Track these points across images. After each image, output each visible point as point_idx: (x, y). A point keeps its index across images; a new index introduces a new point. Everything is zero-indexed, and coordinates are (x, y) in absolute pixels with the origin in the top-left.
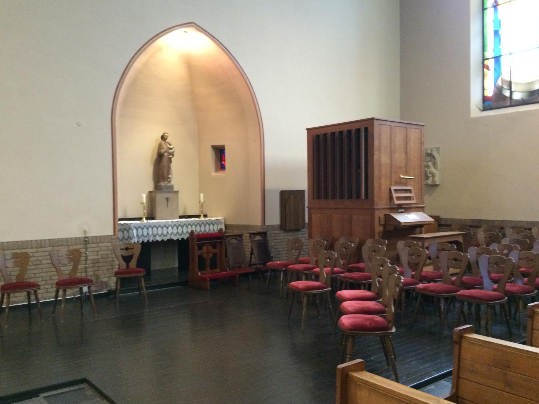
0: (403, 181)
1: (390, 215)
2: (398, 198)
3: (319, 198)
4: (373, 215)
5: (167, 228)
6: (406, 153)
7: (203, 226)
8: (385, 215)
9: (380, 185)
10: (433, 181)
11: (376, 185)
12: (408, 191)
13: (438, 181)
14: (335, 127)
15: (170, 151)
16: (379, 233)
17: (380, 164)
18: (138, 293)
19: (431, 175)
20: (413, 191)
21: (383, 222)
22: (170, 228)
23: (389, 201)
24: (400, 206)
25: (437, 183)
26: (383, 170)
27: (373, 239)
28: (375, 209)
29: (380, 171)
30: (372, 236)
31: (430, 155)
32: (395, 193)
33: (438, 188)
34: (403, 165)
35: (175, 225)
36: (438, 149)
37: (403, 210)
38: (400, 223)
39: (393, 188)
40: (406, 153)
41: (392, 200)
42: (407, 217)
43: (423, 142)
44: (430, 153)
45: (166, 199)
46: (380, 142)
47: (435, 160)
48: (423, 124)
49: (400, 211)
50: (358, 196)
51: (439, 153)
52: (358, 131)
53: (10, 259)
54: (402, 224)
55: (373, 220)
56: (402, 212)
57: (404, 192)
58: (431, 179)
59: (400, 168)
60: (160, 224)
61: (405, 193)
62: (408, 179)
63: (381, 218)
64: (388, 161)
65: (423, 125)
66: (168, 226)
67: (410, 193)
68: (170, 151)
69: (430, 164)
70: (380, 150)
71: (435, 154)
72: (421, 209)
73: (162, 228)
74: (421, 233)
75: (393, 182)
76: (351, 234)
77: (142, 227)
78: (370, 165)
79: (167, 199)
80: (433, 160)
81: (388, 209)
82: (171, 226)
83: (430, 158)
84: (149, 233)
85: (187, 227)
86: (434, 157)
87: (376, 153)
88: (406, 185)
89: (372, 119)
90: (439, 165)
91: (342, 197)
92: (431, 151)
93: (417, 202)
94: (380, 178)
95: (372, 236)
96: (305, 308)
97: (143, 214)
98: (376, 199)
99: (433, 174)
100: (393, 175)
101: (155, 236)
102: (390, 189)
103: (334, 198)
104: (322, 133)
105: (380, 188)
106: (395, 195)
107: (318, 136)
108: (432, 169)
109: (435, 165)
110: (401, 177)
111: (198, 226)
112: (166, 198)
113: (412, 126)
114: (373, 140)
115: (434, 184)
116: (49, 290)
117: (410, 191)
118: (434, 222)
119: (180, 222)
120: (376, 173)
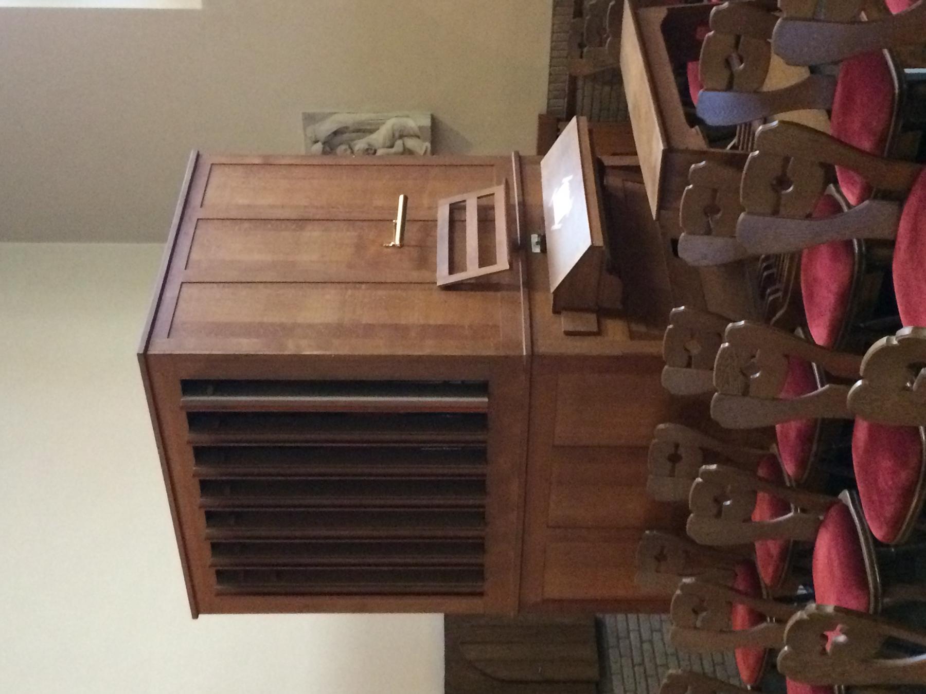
0: (414, 233)
1: (553, 293)
2: (486, 255)
3: (479, 573)
4: (560, 363)
6: (302, 222)
8: (557, 311)
9: (425, 331)
10: (418, 137)
11: (429, 348)
12: (457, 216)
13: (418, 121)
14: (185, 510)
16: (632, 336)
17: (339, 330)
18: (483, 402)
19: (399, 143)
20: (457, 199)
21: (588, 322)
23: (499, 294)
24: (519, 248)
25: (427, 122)
26: (366, 319)
27: (664, 363)
28: (532, 355)
29: (369, 330)
30: (654, 365)
31: (330, 144)
32: (464, 269)
33: (444, 117)
34: (349, 235)
36: (310, 119)
37: (535, 238)
38: (591, 249)
39: (443, 276)
40: (302, 222)
41: (495, 280)
42: (564, 220)
43: (266, 157)
44: (324, 143)
46: (248, 330)
47: (347, 128)
48: (192, 156)
49: (537, 250)
50: (477, 419)
51: (325, 117)
52: (196, 419)
53: (413, 246)
54: (600, 243)
55: (582, 362)
56: (543, 242)
57: (457, 234)
58: (411, 143)
59: (360, 247)
61: (465, 227)
62: (408, 218)
63: (571, 328)
64: (331, 295)
65: (198, 156)
67: (464, 208)
69: (360, 145)
70: (287, 330)
71: (326, 128)
72: (528, 169)
74: (636, 170)
75: (415, 276)
76: (637, 452)
78: (343, 374)
80: (346, 136)
81: (530, 300)
83: (341, 144)
86: (336, 133)
87: (291, 347)
88: (429, 225)
89: (146, 360)
90: (364, 116)
91: (479, 485)
92: (316, 142)
93: (499, 184)
94: (401, 330)
95: (654, 365)
98: (488, 350)
99: (397, 135)
100: (390, 276)
102: (448, 288)
103: (479, 516)
104: (208, 557)
105: (442, 331)
106: (473, 270)
107: (221, 575)
108: (378, 138)
109: (363, 130)
110: (397, 242)
113: (196, 199)
114: (236, 358)
115: (428, 134)
117: (456, 210)
118: (584, 119)
120: (378, 347)
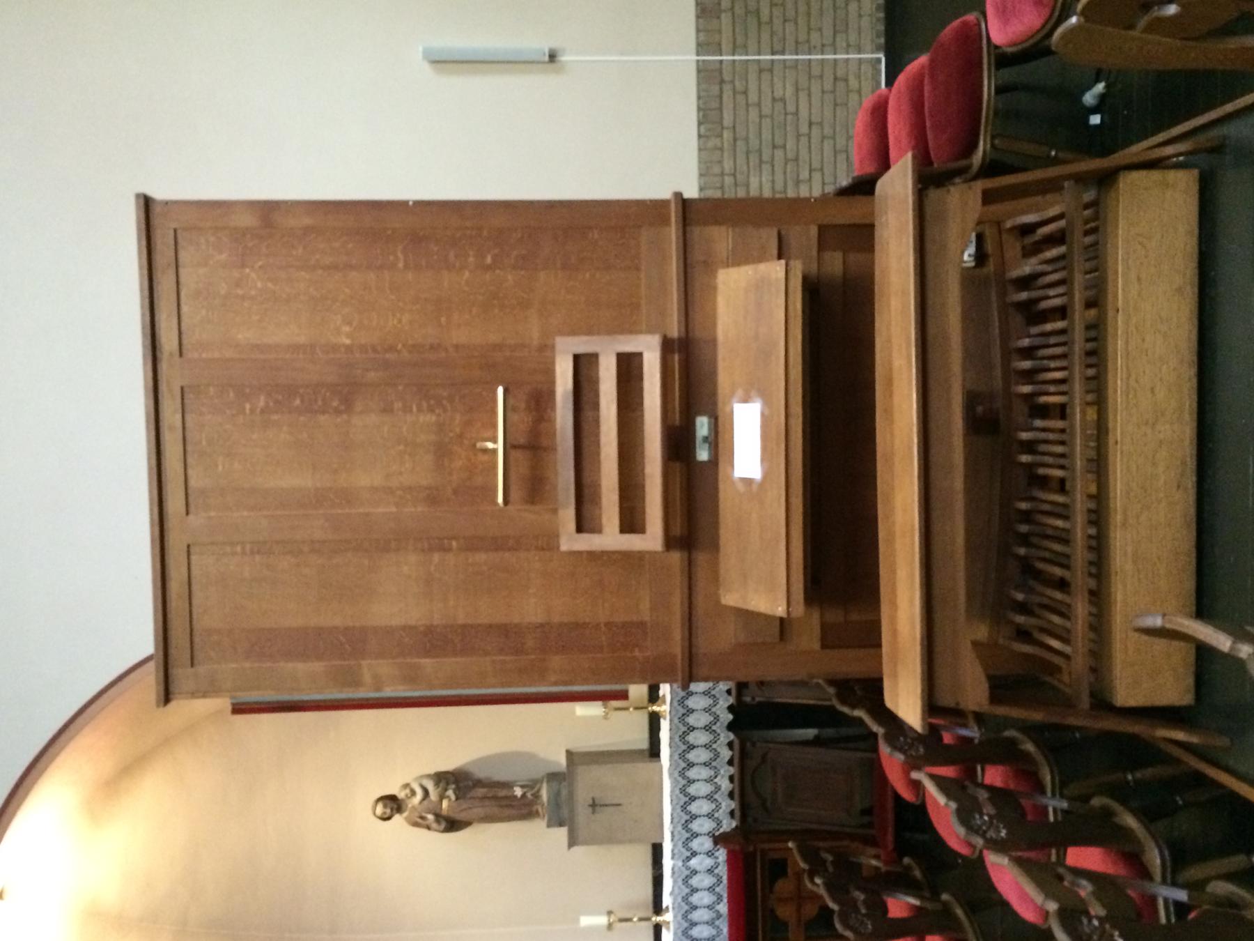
5: (695, 872)
7: (691, 738)
15: (433, 796)
22: (694, 862)
35: (686, 844)
37: (702, 425)
45: (594, 812)
49: (703, 455)
60: (680, 900)
66: (688, 868)
68: (433, 796)
73: (694, 890)
77: (684, 782)
79: (594, 805)
82: (689, 859)
84: (706, 921)
85: (692, 711)
96: (1056, 154)
97: (644, 924)
101: (719, 916)
106: (610, 538)
111: (692, 756)
112: (590, 809)
116: (790, 155)
117: (584, 366)
119: (674, 828)
